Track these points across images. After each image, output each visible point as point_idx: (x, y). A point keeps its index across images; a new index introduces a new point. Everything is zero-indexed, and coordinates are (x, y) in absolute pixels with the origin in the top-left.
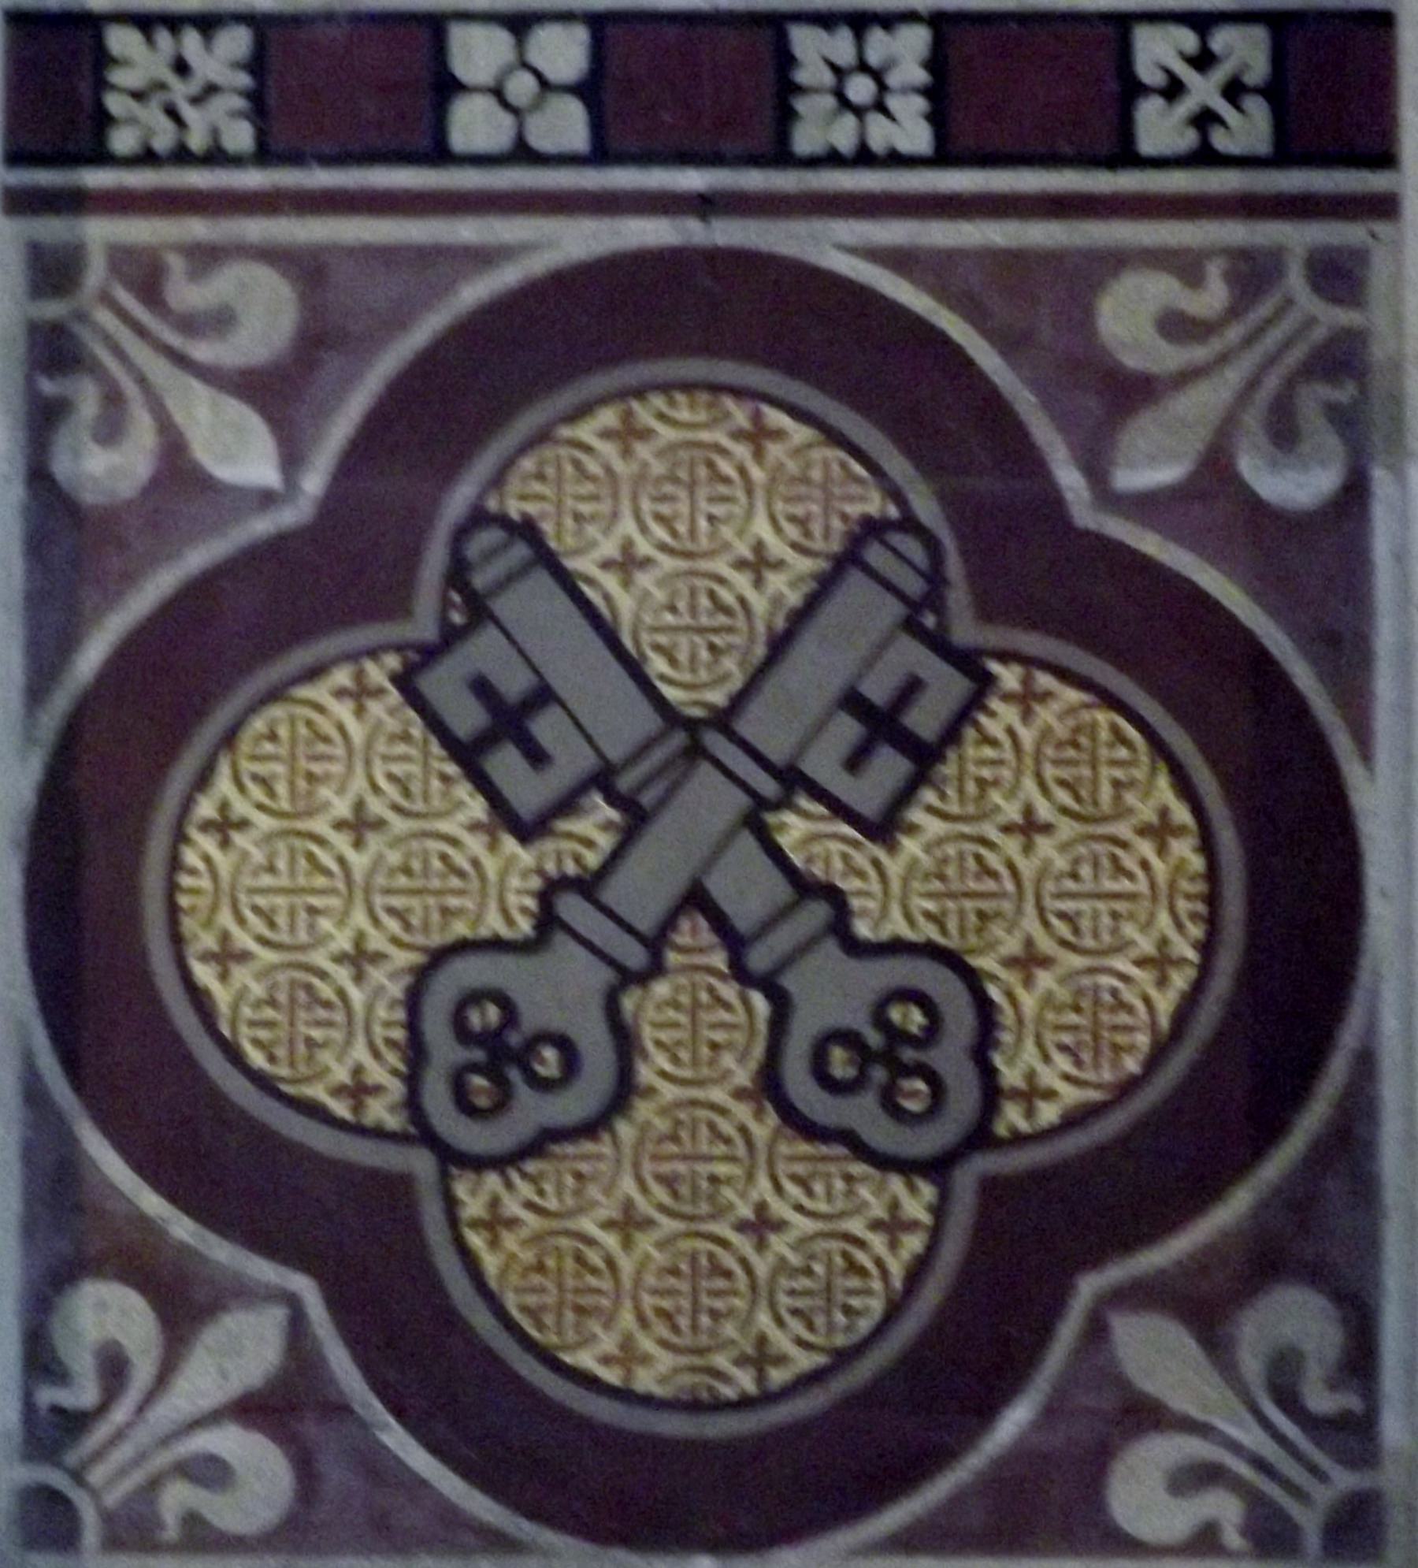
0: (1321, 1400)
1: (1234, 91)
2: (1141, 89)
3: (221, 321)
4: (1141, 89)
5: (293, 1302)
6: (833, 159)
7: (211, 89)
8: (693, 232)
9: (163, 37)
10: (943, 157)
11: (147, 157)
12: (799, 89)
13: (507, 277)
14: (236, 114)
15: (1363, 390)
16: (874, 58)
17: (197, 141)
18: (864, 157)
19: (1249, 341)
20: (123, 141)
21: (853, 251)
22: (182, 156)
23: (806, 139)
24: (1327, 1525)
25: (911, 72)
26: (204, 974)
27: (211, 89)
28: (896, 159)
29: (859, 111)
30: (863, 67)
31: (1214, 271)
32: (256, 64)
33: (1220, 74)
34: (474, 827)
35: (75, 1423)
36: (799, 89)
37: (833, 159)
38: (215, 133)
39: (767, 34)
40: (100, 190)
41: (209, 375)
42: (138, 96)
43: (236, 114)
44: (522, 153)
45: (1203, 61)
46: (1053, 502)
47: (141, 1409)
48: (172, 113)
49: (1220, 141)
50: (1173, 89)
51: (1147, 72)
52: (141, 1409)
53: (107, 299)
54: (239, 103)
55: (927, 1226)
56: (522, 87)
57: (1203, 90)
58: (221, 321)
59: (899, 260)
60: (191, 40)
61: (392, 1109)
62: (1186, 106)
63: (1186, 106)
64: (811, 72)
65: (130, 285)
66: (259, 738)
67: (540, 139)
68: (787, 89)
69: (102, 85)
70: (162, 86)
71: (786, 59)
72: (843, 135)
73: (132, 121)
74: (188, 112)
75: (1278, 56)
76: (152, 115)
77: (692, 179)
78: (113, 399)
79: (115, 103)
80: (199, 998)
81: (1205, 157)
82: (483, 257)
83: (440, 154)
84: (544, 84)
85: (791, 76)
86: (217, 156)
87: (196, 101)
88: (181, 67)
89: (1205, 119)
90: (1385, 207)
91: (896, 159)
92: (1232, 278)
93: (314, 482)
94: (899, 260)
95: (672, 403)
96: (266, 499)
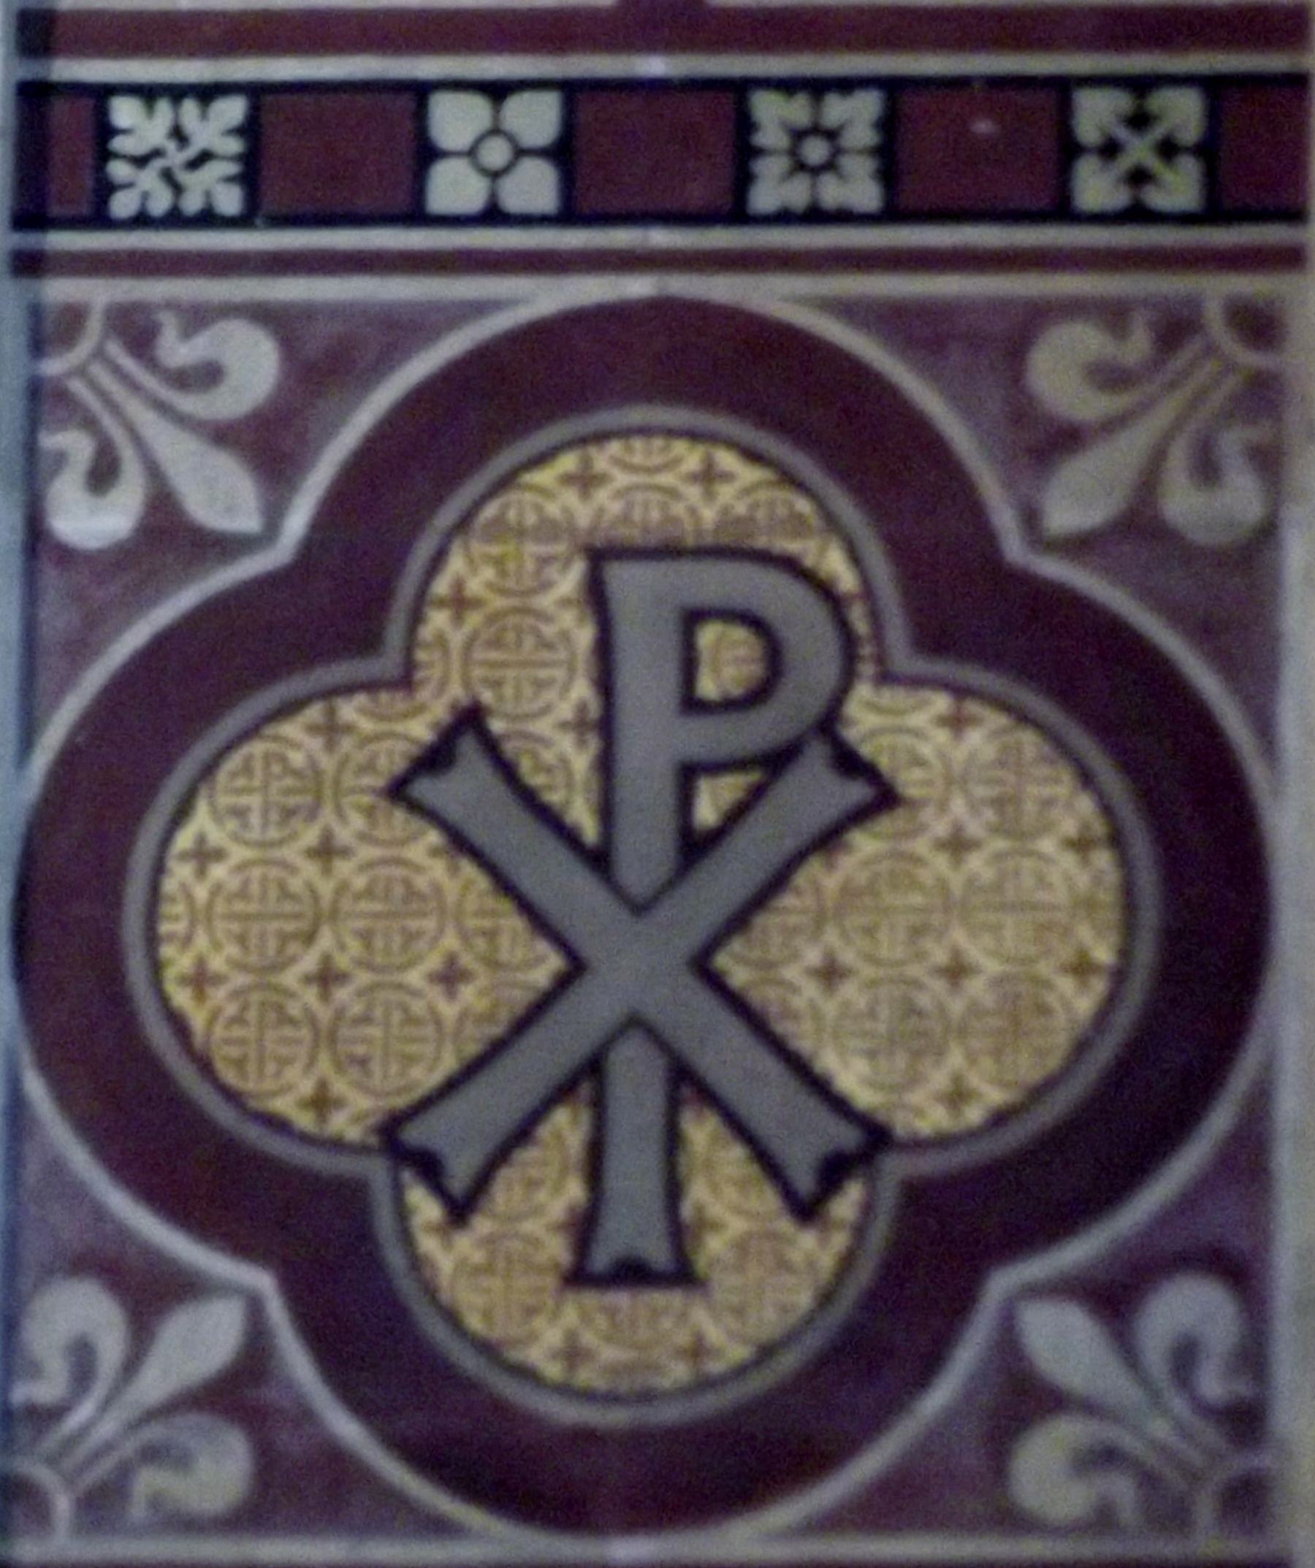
3: (208, 375)
5: (255, 1307)
7: (204, 158)
8: (638, 287)
9: (163, 106)
10: (891, 214)
11: (142, 220)
12: (758, 152)
14: (230, 179)
18: (815, 215)
20: (122, 205)
21: (785, 299)
22: (175, 219)
23: (765, 197)
24: (744, 1504)
26: (181, 998)
28: (844, 217)
32: (250, 130)
34: (434, 852)
36: (758, 152)
38: (208, 194)
39: (88, 103)
42: (141, 161)
43: (230, 179)
44: (493, 215)
45: (1139, 121)
50: (1110, 149)
56: (496, 153)
57: (1139, 151)
58: (208, 375)
59: (847, 310)
60: (190, 108)
64: (770, 134)
66: (234, 775)
67: (1158, 199)
69: (105, 155)
71: (745, 124)
72: (797, 194)
74: (185, 178)
75: (1214, 115)
76: (149, 179)
77: (660, 238)
79: (119, 170)
80: (178, 1024)
81: (1137, 214)
82: (480, 309)
83: (417, 216)
86: (208, 219)
88: (179, 135)
90: (1291, 258)
94: (847, 310)
95: (629, 449)
96: (1036, 1291)
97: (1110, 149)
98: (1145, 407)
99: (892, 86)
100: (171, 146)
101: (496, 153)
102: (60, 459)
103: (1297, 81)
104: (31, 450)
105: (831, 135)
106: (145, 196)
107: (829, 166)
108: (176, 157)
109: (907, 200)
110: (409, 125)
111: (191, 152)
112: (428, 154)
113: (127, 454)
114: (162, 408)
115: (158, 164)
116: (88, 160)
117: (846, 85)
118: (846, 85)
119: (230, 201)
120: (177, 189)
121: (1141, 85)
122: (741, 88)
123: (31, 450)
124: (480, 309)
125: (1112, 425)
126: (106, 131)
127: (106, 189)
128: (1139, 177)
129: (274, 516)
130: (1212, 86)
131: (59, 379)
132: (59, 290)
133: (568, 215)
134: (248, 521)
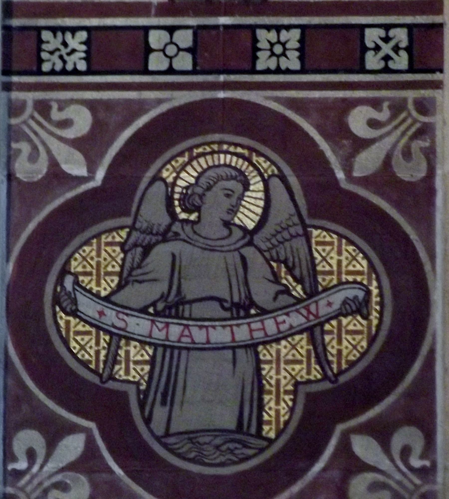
0: (416, 463)
1: (396, 49)
2: (368, 49)
4: (368, 49)
6: (268, 71)
7: (74, 51)
8: (340, 94)
11: (53, 72)
13: (164, 108)
15: (433, 142)
16: (283, 39)
17: (70, 67)
18: (278, 71)
19: (396, 127)
20: (46, 67)
22: (64, 72)
25: (294, 44)
27: (74, 51)
28: (288, 71)
29: (278, 56)
30: (279, 42)
31: (386, 105)
33: (392, 43)
35: (415, 136)
37: (268, 71)
38: (75, 64)
40: (133, 91)
41: (61, 139)
42: (52, 53)
44: (171, 71)
45: (386, 40)
46: (336, 181)
47: (42, 467)
48: (61, 57)
49: (391, 65)
50: (377, 48)
51: (369, 44)
52: (42, 467)
53: (33, 117)
54: (83, 55)
55: (146, 381)
56: (172, 50)
57: (386, 49)
60: (68, 36)
61: (266, 398)
62: (381, 54)
63: (381, 54)
65: (40, 113)
67: (177, 65)
68: (256, 49)
69: (39, 50)
70: (58, 50)
72: (273, 64)
73: (48, 60)
76: (55, 58)
78: (35, 148)
79: (44, 55)
81: (386, 70)
84: (179, 49)
85: (256, 46)
86: (75, 72)
87: (69, 54)
88: (65, 44)
89: (387, 58)
90: (438, 85)
91: (288, 71)
92: (390, 107)
93: (100, 174)
96: (81, 180)
97: (396, 49)
98: (44, 144)
99: (303, 27)
100: (62, 47)
101: (172, 50)
102: (19, 151)
103: (440, 26)
104: (9, 147)
105: (284, 45)
106: (54, 64)
107: (273, 54)
108: (64, 51)
109: (95, 68)
110: (359, 42)
111: (69, 50)
112: (149, 50)
113: (41, 148)
114: (52, 134)
115: (57, 54)
116: (93, 52)
117: (288, 28)
118: (288, 28)
119: (82, 66)
120: (65, 62)
121: (387, 27)
122: (253, 28)
123: (9, 147)
124: (160, 102)
125: (49, 152)
126: (40, 41)
127: (40, 61)
128: (387, 58)
129: (92, 170)
130: (410, 27)
131: (17, 125)
132: (16, 95)
133: (411, 70)
134: (82, 171)
